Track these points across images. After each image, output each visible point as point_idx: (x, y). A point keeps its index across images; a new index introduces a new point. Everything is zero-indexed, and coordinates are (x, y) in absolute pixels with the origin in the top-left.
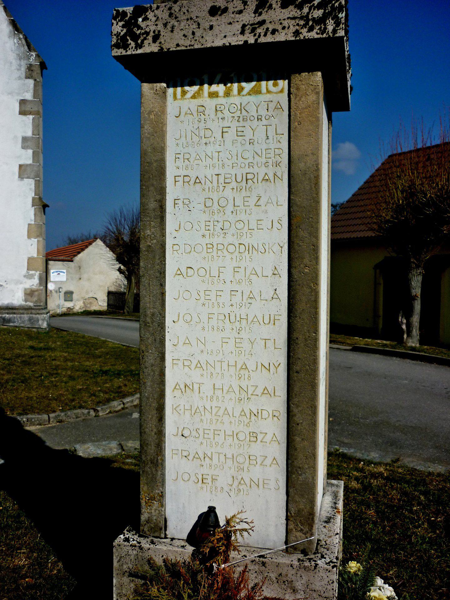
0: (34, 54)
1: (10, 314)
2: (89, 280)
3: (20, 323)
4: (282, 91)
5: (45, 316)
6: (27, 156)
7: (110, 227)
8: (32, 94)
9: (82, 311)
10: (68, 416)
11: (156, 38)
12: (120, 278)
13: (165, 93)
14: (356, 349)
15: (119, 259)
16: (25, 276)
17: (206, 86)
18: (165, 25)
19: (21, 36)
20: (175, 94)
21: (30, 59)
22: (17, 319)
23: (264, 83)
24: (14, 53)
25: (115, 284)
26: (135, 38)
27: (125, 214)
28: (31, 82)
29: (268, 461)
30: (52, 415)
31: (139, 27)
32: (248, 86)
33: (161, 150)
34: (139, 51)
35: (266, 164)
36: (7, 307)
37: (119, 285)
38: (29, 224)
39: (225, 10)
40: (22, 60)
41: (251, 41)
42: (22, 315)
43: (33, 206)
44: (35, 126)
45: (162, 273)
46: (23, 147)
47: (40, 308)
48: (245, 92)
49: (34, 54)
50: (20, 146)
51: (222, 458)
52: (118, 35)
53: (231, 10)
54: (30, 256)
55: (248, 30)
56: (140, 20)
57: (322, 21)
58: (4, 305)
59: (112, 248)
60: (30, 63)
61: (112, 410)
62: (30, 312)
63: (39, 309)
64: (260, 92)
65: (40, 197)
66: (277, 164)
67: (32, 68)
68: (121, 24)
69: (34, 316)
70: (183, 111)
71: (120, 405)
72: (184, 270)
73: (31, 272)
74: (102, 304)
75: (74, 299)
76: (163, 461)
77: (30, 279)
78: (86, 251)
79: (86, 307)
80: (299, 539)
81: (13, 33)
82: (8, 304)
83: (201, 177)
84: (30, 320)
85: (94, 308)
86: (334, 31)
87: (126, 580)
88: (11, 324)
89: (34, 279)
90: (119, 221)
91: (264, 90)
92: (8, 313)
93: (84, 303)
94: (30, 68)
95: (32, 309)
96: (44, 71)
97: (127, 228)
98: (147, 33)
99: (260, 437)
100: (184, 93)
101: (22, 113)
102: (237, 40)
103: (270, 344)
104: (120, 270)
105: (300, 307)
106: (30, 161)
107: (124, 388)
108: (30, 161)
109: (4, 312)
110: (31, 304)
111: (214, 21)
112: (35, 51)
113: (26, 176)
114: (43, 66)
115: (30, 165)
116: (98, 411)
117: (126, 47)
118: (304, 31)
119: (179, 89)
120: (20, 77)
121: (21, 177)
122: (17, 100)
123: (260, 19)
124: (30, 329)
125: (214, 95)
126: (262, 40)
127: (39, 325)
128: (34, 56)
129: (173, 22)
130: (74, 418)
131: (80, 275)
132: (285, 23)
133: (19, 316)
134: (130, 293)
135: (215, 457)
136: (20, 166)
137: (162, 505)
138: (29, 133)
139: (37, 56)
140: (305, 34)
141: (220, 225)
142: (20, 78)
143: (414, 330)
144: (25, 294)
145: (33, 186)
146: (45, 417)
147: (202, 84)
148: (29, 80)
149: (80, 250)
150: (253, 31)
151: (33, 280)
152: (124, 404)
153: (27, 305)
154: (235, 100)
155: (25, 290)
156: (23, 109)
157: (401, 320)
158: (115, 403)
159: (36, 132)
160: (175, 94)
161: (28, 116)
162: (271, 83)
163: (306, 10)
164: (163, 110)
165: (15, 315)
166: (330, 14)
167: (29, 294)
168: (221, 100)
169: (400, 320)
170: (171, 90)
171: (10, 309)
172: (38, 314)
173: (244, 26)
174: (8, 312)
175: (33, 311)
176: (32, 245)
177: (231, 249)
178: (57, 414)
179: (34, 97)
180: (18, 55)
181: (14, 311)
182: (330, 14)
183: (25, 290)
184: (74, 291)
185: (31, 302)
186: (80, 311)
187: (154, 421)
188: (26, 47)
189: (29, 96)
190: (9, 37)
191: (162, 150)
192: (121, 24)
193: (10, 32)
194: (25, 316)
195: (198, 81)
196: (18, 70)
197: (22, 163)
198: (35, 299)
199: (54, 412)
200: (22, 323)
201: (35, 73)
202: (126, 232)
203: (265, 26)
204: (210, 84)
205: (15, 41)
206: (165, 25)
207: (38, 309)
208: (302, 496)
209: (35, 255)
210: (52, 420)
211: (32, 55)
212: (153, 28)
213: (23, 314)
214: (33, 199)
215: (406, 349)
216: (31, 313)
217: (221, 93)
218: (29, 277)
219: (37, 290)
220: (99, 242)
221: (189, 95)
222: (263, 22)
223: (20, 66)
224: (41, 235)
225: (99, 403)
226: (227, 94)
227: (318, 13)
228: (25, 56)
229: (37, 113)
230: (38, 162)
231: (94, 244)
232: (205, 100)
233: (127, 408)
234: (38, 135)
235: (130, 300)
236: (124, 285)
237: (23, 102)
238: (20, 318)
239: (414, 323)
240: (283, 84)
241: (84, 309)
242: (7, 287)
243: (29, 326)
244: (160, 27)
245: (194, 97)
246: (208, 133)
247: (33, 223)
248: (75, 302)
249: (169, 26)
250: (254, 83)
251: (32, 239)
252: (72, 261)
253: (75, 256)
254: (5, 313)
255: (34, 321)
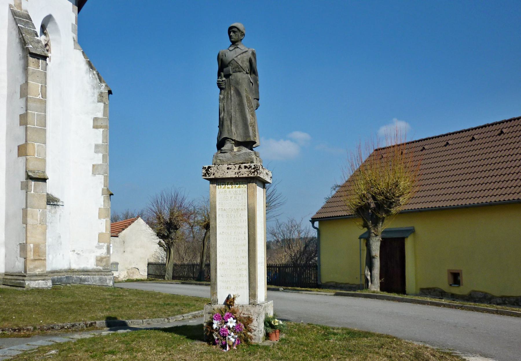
0: (104, 85)
1: (86, 275)
2: (132, 252)
3: (93, 282)
4: (245, 187)
5: (111, 276)
6: (98, 159)
7: (153, 208)
8: (103, 113)
9: (126, 279)
10: (153, 321)
11: (214, 174)
12: (158, 251)
13: (216, 187)
14: (337, 294)
15: (159, 235)
16: (96, 247)
17: (226, 185)
18: (216, 171)
19: (95, 72)
20: (218, 187)
21: (101, 88)
22: (91, 279)
23: (241, 185)
24: (89, 84)
25: (154, 256)
26: (208, 174)
27: (165, 197)
28: (101, 105)
29: (244, 282)
30: (145, 320)
31: (209, 171)
32: (237, 186)
33: (215, 202)
34: (209, 177)
35: (242, 206)
36: (83, 270)
37: (158, 256)
38: (100, 208)
39: (231, 168)
40: (95, 90)
41: (237, 176)
42: (94, 276)
43: (102, 195)
44: (104, 137)
45: (216, 234)
46: (96, 152)
47: (108, 270)
48: (236, 187)
49: (104, 85)
50: (94, 151)
51: (232, 281)
52: (204, 173)
53: (232, 168)
54: (100, 232)
55: (236, 173)
56: (209, 169)
57: (254, 172)
58: (81, 269)
59: (151, 225)
60: (100, 91)
61: (177, 319)
62: (100, 274)
63: (107, 272)
64: (240, 188)
65: (107, 188)
66: (245, 206)
67: (103, 95)
68: (205, 170)
69: (103, 276)
70: (221, 192)
71: (181, 317)
72: (222, 233)
73: (101, 244)
74: (143, 274)
75: (119, 269)
76: (217, 283)
77: (101, 249)
78: (130, 227)
79: (129, 276)
80: (252, 301)
81: (89, 70)
82: (84, 268)
83: (226, 209)
84: (100, 279)
85: (135, 277)
86: (257, 175)
87: (207, 315)
88: (86, 283)
89: (103, 249)
90: (160, 203)
91: (241, 187)
92: (84, 275)
93: (127, 272)
94: (101, 95)
95: (101, 271)
96: (110, 95)
97: (167, 209)
98: (211, 173)
99: (242, 275)
100: (221, 187)
101: (95, 127)
102: (234, 176)
103: (244, 251)
104: (160, 244)
105: (251, 241)
106: (100, 162)
107: (181, 311)
108: (100, 162)
109: (81, 274)
110: (101, 268)
111: (228, 171)
112: (104, 82)
113: (97, 173)
114: (110, 92)
115: (101, 164)
116: (169, 319)
117: (206, 176)
118: (250, 174)
119: (220, 186)
120: (93, 101)
121: (94, 173)
122: (92, 118)
123: (239, 171)
124: (100, 286)
125: (228, 188)
126: (240, 176)
127: (107, 283)
128: (104, 86)
129: (218, 170)
130: (156, 323)
131: (124, 248)
132: (245, 172)
133: (92, 276)
134: (169, 262)
135: (231, 282)
136: (93, 166)
137: (217, 295)
138: (100, 142)
139: (106, 86)
140: (250, 175)
141: (231, 221)
142: (94, 102)
143: (376, 279)
144: (97, 260)
145: (103, 181)
146: (141, 321)
147: (225, 185)
148: (100, 103)
149: (124, 227)
150: (238, 174)
151: (102, 250)
152: (183, 317)
153: (98, 269)
154: (234, 189)
155: (97, 257)
156: (96, 124)
157: (367, 273)
158: (179, 316)
159: (105, 141)
160: (218, 187)
161: (99, 129)
162: (243, 185)
163: (250, 169)
164: (215, 192)
165: (89, 276)
166: (256, 171)
167: (100, 260)
168: (230, 189)
169: (366, 273)
170: (217, 186)
171: (85, 271)
172: (106, 275)
173: (235, 173)
174: (84, 274)
175: (103, 273)
176: (101, 224)
177: (234, 227)
178: (147, 319)
179: (104, 116)
180: (93, 86)
181: (88, 273)
182: (256, 171)
183: (97, 257)
184: (119, 263)
185: (101, 266)
186: (124, 280)
187: (214, 273)
188: (98, 80)
189: (100, 115)
190: (86, 73)
191: (215, 202)
192: (205, 170)
193: (87, 70)
194: (97, 276)
195: (224, 184)
196: (92, 96)
197: (94, 163)
198: (104, 264)
199: (145, 319)
200: (94, 282)
201: (105, 98)
202: (166, 212)
203: (240, 173)
204: (228, 185)
205: (91, 76)
206: (216, 171)
207: (106, 271)
208: (253, 290)
209: (104, 231)
210: (144, 323)
211: (102, 86)
212: (213, 172)
213: (95, 275)
214: (103, 190)
215: (369, 292)
216: (101, 275)
217: (230, 188)
218: (99, 247)
219: (105, 258)
220: (140, 221)
221: (222, 188)
222: (240, 172)
223: (94, 93)
224: (109, 216)
225: (169, 316)
226: (232, 188)
227: (253, 170)
228: (98, 86)
229: (106, 127)
230: (106, 162)
231: (136, 222)
232: (226, 189)
233: (185, 319)
234: (107, 143)
235: (169, 269)
236: (162, 257)
237: (95, 119)
238: (93, 278)
239: (375, 275)
240: (246, 186)
241: (128, 278)
242: (83, 255)
243: (99, 284)
244: (215, 172)
245: (223, 188)
246: (227, 198)
247: (103, 207)
248: (120, 271)
249: (217, 171)
250: (238, 185)
251: (102, 219)
252: (117, 237)
253: (120, 232)
254: (82, 275)
255: (103, 280)
